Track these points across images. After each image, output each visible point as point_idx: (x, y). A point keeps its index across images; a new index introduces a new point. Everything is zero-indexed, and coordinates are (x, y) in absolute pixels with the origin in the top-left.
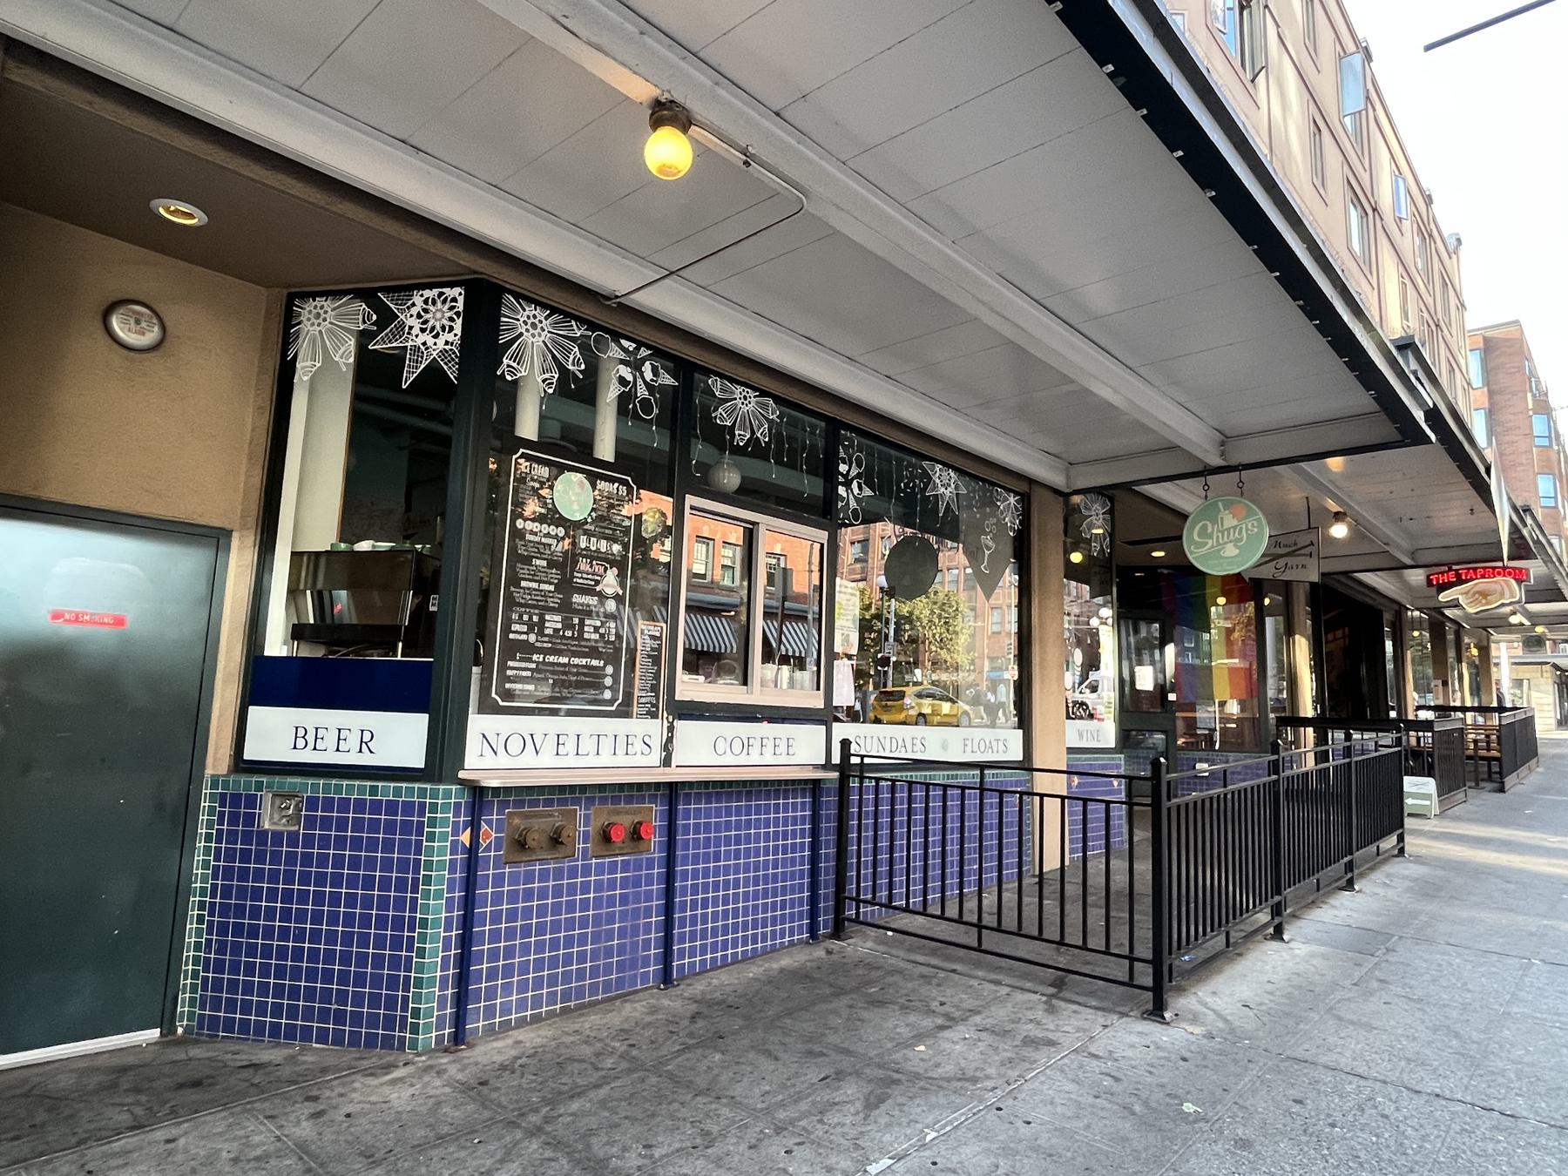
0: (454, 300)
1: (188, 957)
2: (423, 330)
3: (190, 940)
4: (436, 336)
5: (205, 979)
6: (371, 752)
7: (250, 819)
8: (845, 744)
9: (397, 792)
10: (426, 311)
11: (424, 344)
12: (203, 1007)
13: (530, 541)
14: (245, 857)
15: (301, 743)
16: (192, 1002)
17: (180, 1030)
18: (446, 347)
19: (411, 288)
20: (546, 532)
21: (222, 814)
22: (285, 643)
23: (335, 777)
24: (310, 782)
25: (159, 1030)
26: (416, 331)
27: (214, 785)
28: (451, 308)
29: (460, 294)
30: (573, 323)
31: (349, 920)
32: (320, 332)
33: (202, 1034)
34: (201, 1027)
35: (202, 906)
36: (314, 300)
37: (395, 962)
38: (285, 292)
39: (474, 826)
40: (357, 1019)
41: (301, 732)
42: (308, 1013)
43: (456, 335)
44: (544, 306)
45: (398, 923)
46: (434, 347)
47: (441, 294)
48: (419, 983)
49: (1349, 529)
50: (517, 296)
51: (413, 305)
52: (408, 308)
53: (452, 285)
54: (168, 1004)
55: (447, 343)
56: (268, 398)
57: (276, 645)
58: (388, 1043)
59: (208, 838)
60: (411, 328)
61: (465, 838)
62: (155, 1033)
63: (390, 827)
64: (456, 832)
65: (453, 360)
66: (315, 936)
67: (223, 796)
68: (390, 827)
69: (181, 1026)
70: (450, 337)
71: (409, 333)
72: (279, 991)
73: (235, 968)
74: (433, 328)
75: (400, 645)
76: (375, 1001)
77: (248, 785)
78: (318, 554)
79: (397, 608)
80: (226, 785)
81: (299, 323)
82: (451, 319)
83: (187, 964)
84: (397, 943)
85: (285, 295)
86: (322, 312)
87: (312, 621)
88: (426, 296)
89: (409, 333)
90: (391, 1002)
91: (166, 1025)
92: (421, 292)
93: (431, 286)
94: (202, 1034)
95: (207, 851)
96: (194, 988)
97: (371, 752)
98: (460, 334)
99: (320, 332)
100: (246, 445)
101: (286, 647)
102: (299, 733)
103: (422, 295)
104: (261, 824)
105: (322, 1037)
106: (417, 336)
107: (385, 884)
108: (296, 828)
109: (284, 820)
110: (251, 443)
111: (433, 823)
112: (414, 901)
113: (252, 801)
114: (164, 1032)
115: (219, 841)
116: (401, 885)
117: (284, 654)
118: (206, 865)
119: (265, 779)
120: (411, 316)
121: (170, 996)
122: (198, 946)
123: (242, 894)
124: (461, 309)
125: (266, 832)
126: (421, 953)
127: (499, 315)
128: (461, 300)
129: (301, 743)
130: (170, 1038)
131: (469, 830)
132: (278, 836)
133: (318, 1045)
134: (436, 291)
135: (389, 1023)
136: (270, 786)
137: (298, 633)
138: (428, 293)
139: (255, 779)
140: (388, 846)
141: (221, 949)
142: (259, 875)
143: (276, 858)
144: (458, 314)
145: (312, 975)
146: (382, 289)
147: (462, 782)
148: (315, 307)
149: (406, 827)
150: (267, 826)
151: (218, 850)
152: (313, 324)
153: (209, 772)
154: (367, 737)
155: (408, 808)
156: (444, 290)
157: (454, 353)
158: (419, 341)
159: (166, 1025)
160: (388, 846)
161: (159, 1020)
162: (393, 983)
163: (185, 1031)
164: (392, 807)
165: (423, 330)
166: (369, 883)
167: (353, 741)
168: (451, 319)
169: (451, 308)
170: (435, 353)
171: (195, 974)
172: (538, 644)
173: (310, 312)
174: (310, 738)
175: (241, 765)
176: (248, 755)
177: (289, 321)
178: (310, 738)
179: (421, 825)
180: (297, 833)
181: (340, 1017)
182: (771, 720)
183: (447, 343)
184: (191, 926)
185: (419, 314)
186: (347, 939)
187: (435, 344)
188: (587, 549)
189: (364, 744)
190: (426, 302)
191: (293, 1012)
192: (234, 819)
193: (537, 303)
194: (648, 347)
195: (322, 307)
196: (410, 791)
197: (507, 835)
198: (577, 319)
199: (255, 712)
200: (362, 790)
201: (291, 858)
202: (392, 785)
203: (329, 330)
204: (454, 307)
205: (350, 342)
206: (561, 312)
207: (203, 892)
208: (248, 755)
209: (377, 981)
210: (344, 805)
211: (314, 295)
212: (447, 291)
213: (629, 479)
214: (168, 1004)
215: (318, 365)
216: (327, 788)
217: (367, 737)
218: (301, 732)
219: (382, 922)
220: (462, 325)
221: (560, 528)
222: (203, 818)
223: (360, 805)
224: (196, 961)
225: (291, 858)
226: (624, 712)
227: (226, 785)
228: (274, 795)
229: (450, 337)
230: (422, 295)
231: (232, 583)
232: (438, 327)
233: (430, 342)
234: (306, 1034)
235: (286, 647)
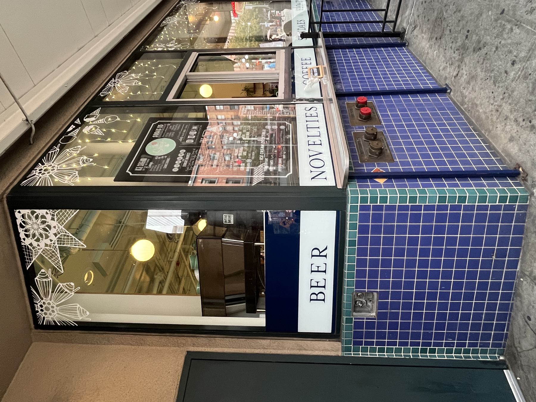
0: (23, 216)
1: (456, 357)
2: (47, 237)
3: (445, 356)
4: (49, 227)
5: (470, 345)
6: (326, 249)
7: (370, 325)
8: (304, 36)
9: (353, 227)
10: (34, 236)
11: (55, 235)
12: (487, 345)
13: (187, 164)
14: (394, 326)
15: (321, 296)
16: (484, 352)
17: (502, 358)
18: (56, 219)
19: (20, 247)
20: (182, 158)
21: (367, 343)
22: (258, 317)
23: (343, 271)
24: (346, 287)
25: (504, 371)
26: (48, 241)
27: (348, 349)
28: (30, 218)
29: (19, 212)
30: (50, 152)
31: (437, 253)
32: (57, 306)
33: (505, 344)
34: (499, 345)
35: (424, 351)
36: (38, 312)
37: (468, 218)
38: (34, 331)
39: (372, 177)
40: (503, 242)
41: (314, 297)
42: (497, 275)
43: (47, 213)
44: (36, 165)
45: (441, 218)
46: (57, 228)
47: (22, 226)
48: (483, 199)
49: (219, 20)
50: (25, 178)
51: (31, 244)
52: (34, 248)
53: (14, 219)
54: (486, 366)
55: (53, 219)
56: (102, 336)
57: (260, 321)
58: (521, 218)
59: (381, 350)
60: (46, 245)
61: (381, 181)
62: (507, 373)
63: (376, 229)
64: (379, 186)
65: (63, 213)
66: (447, 275)
67: (355, 343)
68: (376, 229)
69: (499, 357)
70: (49, 217)
71: (50, 246)
72: (481, 296)
73: (464, 327)
74: (45, 230)
75: (256, 244)
76: (492, 230)
77: (348, 328)
78: (203, 303)
79: (233, 247)
80: (348, 342)
81: (54, 322)
82: (37, 217)
83: (461, 357)
84: (455, 218)
85: (36, 331)
86: (44, 306)
87: (245, 304)
88: (24, 237)
89: (50, 246)
90: (495, 218)
91: (501, 367)
92: (22, 240)
93: (17, 234)
94: (505, 344)
95: (390, 351)
96: (475, 352)
97: (326, 249)
98: (46, 210)
99: (57, 306)
100: (133, 347)
101: (260, 315)
102: (315, 298)
103: (24, 239)
104: (373, 317)
105: (513, 264)
106: (51, 241)
107: (414, 230)
108: (375, 294)
109: (369, 304)
110: (131, 345)
111: (374, 199)
112: (427, 208)
113: (359, 325)
114: (505, 367)
115: (383, 344)
116: (416, 218)
117: (264, 316)
118: (398, 351)
119: (344, 318)
120: (38, 245)
121: (483, 366)
122: (449, 352)
123: (417, 326)
124: (29, 211)
125: (379, 314)
126: (462, 199)
127: (35, 187)
128: (23, 211)
129: (321, 296)
130: (507, 363)
131: (377, 180)
132: (381, 306)
133: (519, 267)
134: (20, 230)
135: (508, 218)
136: (348, 314)
137: (251, 311)
138: (22, 235)
139: (344, 324)
140: (389, 230)
141: (451, 336)
142: (406, 316)
143: (395, 306)
144: (33, 213)
145: (471, 275)
146: (24, 267)
147: (345, 186)
148: (42, 310)
149: (377, 218)
150: (374, 314)
151: (389, 344)
152: (53, 311)
153: (340, 354)
154: (316, 252)
155: (364, 218)
156: (18, 224)
157: (59, 213)
158: (54, 239)
159: (501, 367)
160: (389, 230)
161: (502, 370)
162: (481, 218)
163: (502, 354)
164: (363, 230)
165: (47, 237)
166: (413, 241)
167: (319, 262)
168: (37, 217)
169: (30, 218)
170: (61, 227)
171: (467, 352)
172: (253, 158)
173: (46, 314)
174: (316, 291)
175: (335, 334)
176: (327, 329)
177: (53, 327)
178: (316, 291)
179: (376, 208)
180: (379, 293)
181: (502, 254)
182: (293, 69)
183: (53, 219)
184: (437, 356)
185: (36, 240)
186: (450, 253)
187: (55, 227)
188: (194, 139)
189: (321, 254)
190: (27, 236)
191: (495, 286)
192: (370, 335)
193: (33, 168)
194: (75, 119)
195: (41, 306)
196: (353, 217)
197: (376, 161)
198: (49, 149)
199: (302, 328)
200: (351, 252)
201: (396, 296)
202: (348, 231)
203: (56, 300)
204: (29, 216)
205: (61, 286)
206: (42, 157)
207: (415, 351)
208: (327, 329)
209: (479, 230)
210: (361, 263)
211: (34, 312)
212: (19, 221)
213: (153, 124)
214: (486, 366)
215: (78, 306)
216: (350, 276)
217: (316, 252)
218: (314, 297)
219: (440, 230)
220: (39, 209)
221: (181, 151)
222: (369, 355)
223: (362, 252)
224: (458, 352)
225: (396, 296)
226: (294, 119)
227: (348, 342)
228: (355, 311)
229: (49, 217)
230: (24, 239)
231: (221, 349)
232: (43, 226)
233: (53, 231)
234: (511, 276)
235: (260, 315)
